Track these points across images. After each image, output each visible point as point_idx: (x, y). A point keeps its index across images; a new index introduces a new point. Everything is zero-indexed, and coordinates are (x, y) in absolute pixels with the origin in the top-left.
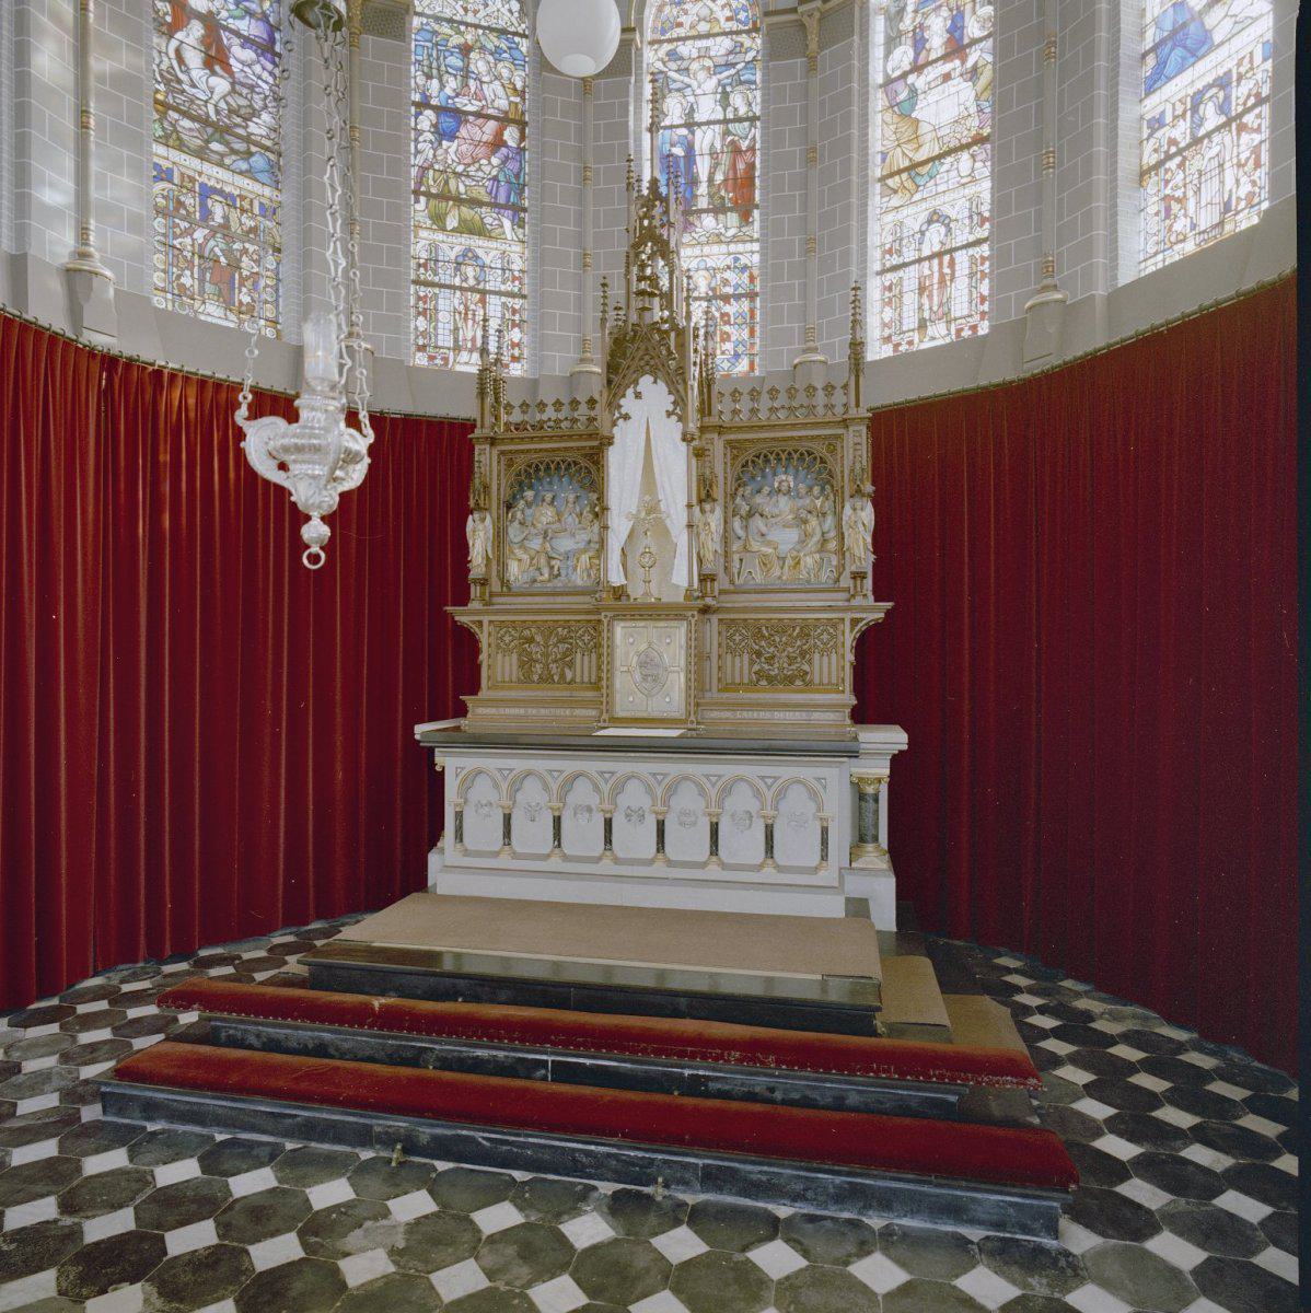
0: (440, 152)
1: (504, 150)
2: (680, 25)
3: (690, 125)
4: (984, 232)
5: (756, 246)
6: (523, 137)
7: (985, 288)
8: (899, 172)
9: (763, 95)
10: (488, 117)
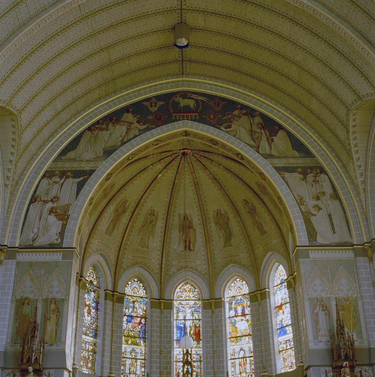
0: (128, 326)
1: (141, 324)
2: (182, 297)
3: (185, 320)
4: (252, 355)
5: (201, 349)
6: (146, 321)
7: (253, 367)
8: (233, 337)
9: (202, 315)
10: (138, 317)
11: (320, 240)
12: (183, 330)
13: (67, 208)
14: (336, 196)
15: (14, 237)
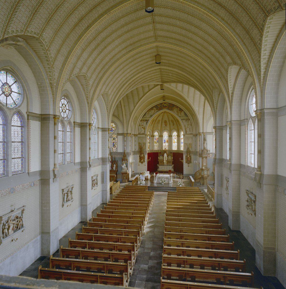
11: (187, 133)
12: (165, 141)
13: (145, 127)
14: (191, 125)
15: (137, 132)
